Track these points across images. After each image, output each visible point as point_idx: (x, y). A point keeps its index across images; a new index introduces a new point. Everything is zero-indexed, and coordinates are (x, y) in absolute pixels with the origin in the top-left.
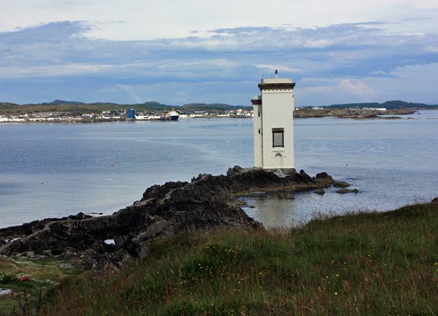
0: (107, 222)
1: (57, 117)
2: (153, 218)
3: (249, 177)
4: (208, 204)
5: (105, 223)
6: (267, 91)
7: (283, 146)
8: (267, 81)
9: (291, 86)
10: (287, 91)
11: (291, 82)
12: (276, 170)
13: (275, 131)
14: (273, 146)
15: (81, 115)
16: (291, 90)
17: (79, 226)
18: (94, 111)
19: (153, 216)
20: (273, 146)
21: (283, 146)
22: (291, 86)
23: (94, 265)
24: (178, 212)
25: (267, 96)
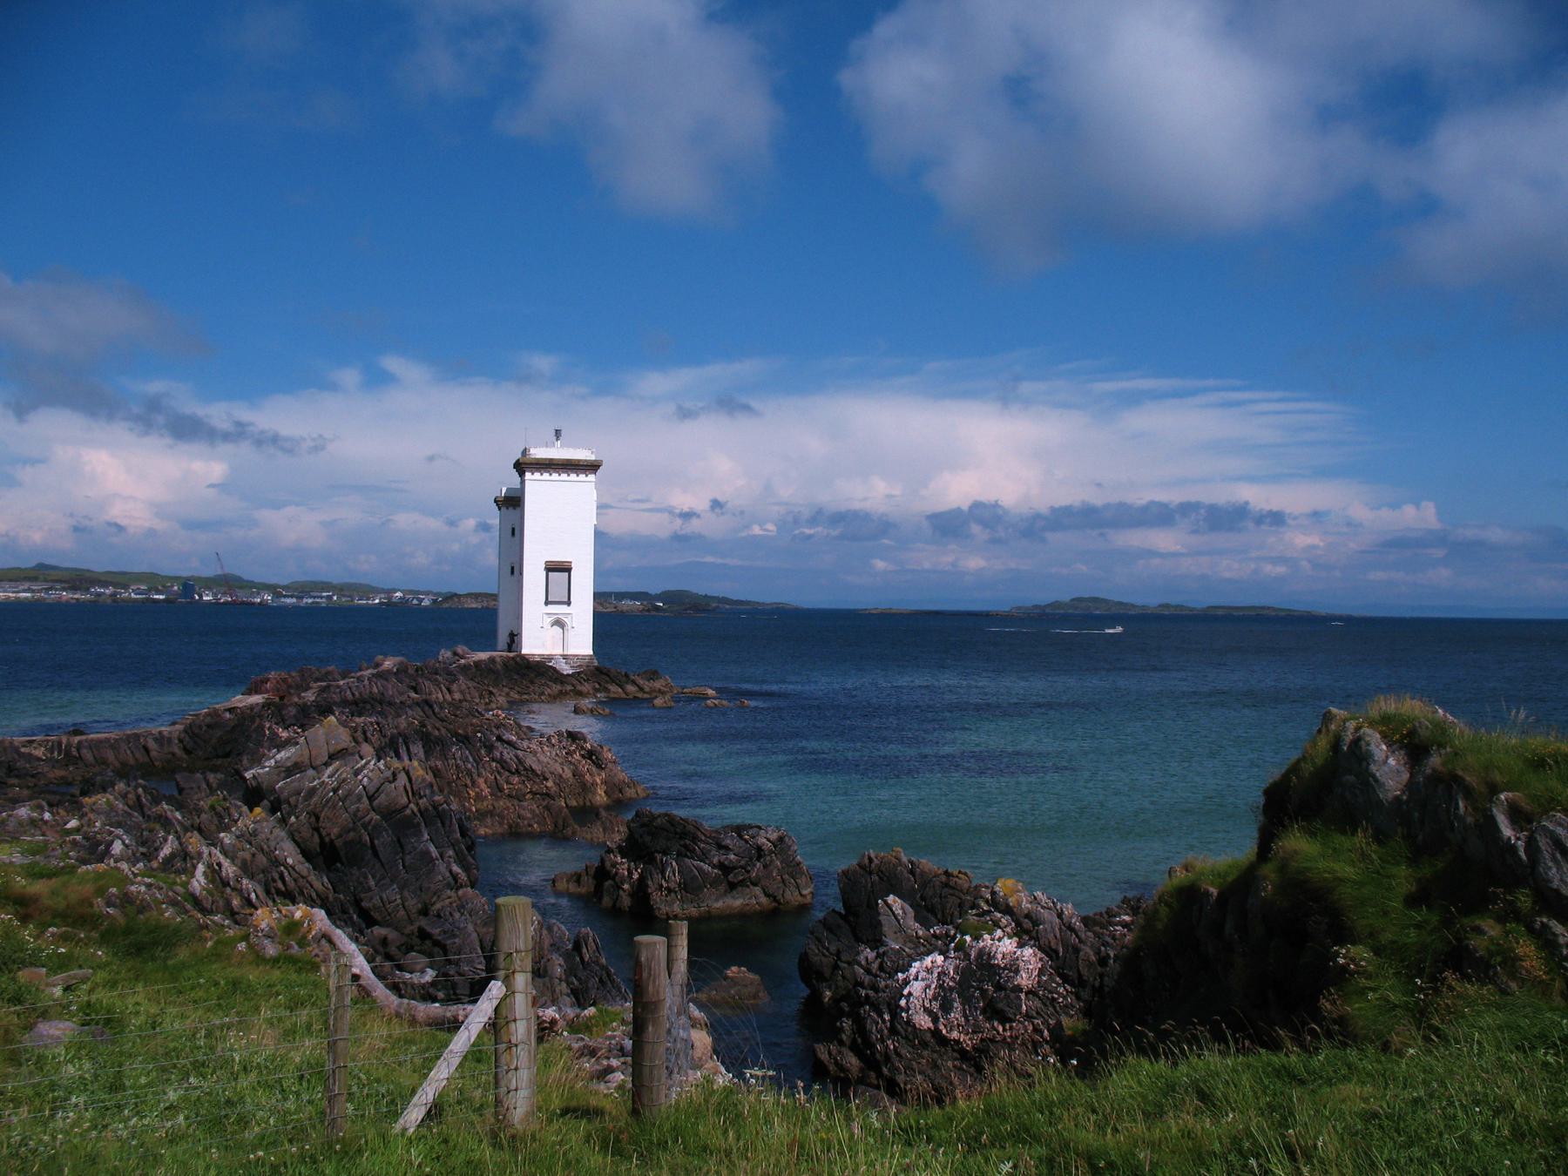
0: (152, 744)
1: (40, 591)
2: (285, 735)
3: (491, 671)
4: (431, 707)
5: (146, 749)
6: (537, 475)
7: (569, 603)
8: (539, 453)
9: (591, 467)
10: (582, 477)
11: (593, 458)
12: (550, 657)
13: (553, 568)
14: (547, 603)
15: (88, 589)
16: (592, 477)
17: (68, 753)
18: (115, 585)
19: (286, 728)
20: (547, 603)
21: (569, 603)
22: (591, 467)
23: (117, 847)
24: (357, 719)
25: (537, 487)
